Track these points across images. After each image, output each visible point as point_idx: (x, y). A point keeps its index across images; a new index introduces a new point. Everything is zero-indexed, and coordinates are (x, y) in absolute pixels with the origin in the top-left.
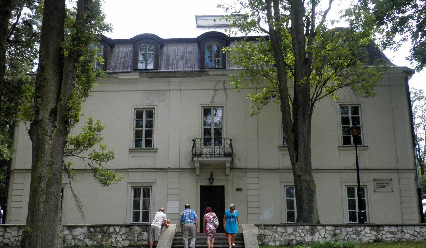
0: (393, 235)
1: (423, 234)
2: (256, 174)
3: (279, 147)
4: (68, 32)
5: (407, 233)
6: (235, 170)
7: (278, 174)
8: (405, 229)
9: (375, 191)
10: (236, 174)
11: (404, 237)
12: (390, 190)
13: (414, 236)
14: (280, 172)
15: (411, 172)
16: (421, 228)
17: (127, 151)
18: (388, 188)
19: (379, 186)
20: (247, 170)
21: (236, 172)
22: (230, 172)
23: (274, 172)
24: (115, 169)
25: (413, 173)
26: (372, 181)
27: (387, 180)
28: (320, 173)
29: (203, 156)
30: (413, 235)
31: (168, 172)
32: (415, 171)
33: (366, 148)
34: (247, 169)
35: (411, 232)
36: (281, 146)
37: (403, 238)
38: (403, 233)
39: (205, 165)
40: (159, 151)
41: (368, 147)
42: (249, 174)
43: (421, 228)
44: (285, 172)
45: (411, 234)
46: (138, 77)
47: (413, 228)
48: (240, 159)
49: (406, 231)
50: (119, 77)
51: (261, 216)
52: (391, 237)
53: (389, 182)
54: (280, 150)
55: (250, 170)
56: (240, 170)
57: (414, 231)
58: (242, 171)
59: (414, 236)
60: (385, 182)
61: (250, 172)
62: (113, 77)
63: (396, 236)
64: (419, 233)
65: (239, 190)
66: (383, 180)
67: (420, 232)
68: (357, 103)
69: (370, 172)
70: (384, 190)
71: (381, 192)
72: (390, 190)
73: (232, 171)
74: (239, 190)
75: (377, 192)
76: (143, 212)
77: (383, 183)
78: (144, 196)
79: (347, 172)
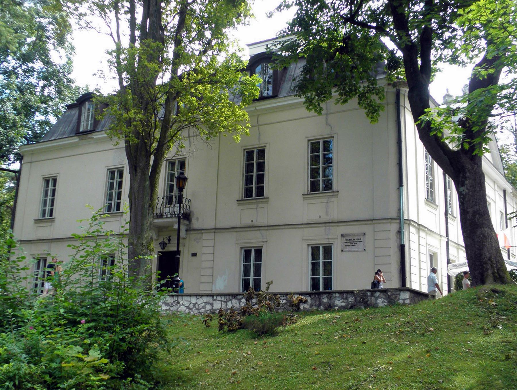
0: (168, 308)
1: (198, 305)
2: (211, 236)
3: (303, 195)
4: (448, 16)
5: (183, 305)
6: (192, 232)
7: (235, 234)
8: (181, 299)
9: (342, 251)
10: (193, 236)
11: (179, 309)
12: (362, 248)
13: (190, 309)
14: (236, 232)
15: (390, 223)
16: (197, 299)
17: (33, 222)
18: (360, 246)
19: (349, 244)
20: (202, 231)
21: (193, 234)
22: (186, 234)
23: (230, 232)
24: (21, 241)
25: (396, 223)
26: (340, 236)
27: (358, 235)
28: (280, 230)
29: (164, 217)
30: (188, 307)
31: (202, 233)
32: (398, 221)
33: (335, 194)
34: (203, 230)
35: (187, 304)
36: (240, 199)
37: (178, 311)
38: (178, 305)
39: (164, 227)
40: (56, 220)
41: (268, 198)
42: (205, 236)
43: (197, 299)
44: (242, 231)
45: (186, 307)
46: (77, 140)
47: (189, 298)
48: (197, 219)
49: (181, 303)
50: (94, 137)
51: (213, 286)
52: (166, 310)
53: (361, 237)
54: (239, 205)
55: (206, 231)
56: (196, 232)
57: (189, 303)
58: (198, 232)
59: (190, 309)
60: (356, 238)
61: (206, 233)
62: (89, 138)
63: (171, 309)
64: (194, 305)
65: (194, 255)
66: (354, 235)
67: (196, 303)
68: (330, 136)
69: (337, 226)
70: (354, 248)
71: (349, 251)
72: (362, 249)
73: (188, 232)
74: (194, 255)
75: (345, 251)
76: (324, 279)
77: (354, 240)
78: (256, 260)
79: (349, 225)
